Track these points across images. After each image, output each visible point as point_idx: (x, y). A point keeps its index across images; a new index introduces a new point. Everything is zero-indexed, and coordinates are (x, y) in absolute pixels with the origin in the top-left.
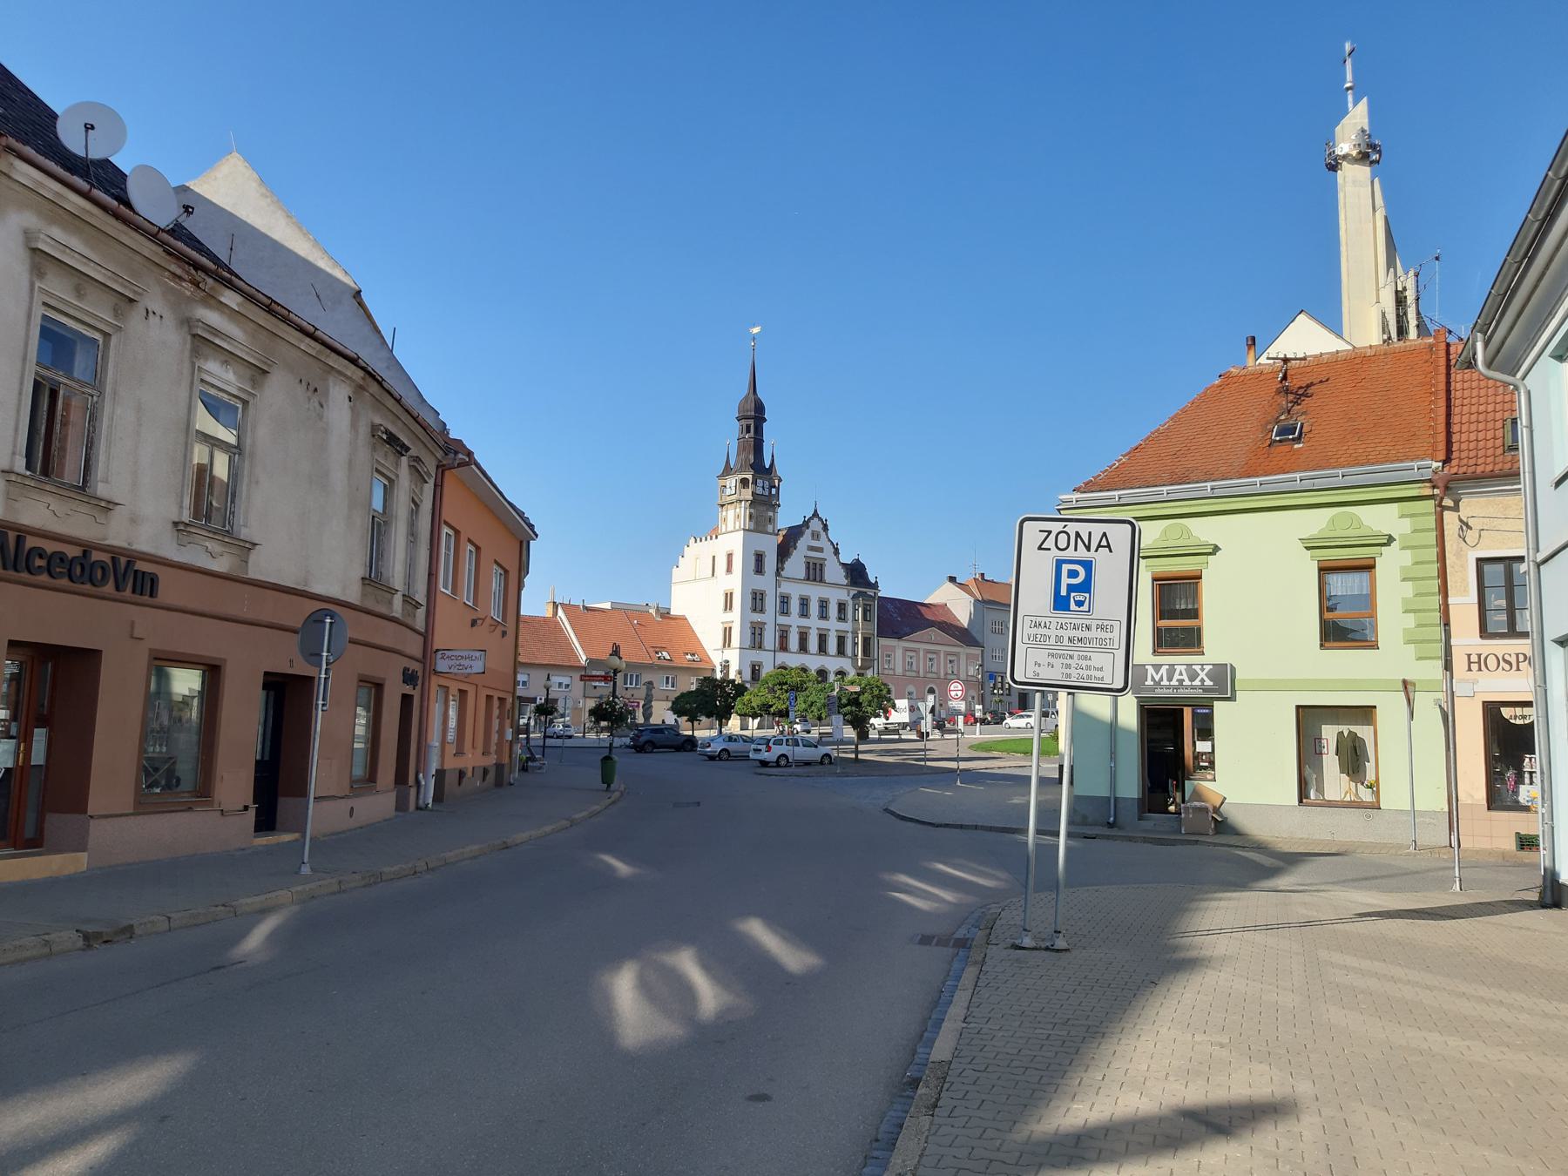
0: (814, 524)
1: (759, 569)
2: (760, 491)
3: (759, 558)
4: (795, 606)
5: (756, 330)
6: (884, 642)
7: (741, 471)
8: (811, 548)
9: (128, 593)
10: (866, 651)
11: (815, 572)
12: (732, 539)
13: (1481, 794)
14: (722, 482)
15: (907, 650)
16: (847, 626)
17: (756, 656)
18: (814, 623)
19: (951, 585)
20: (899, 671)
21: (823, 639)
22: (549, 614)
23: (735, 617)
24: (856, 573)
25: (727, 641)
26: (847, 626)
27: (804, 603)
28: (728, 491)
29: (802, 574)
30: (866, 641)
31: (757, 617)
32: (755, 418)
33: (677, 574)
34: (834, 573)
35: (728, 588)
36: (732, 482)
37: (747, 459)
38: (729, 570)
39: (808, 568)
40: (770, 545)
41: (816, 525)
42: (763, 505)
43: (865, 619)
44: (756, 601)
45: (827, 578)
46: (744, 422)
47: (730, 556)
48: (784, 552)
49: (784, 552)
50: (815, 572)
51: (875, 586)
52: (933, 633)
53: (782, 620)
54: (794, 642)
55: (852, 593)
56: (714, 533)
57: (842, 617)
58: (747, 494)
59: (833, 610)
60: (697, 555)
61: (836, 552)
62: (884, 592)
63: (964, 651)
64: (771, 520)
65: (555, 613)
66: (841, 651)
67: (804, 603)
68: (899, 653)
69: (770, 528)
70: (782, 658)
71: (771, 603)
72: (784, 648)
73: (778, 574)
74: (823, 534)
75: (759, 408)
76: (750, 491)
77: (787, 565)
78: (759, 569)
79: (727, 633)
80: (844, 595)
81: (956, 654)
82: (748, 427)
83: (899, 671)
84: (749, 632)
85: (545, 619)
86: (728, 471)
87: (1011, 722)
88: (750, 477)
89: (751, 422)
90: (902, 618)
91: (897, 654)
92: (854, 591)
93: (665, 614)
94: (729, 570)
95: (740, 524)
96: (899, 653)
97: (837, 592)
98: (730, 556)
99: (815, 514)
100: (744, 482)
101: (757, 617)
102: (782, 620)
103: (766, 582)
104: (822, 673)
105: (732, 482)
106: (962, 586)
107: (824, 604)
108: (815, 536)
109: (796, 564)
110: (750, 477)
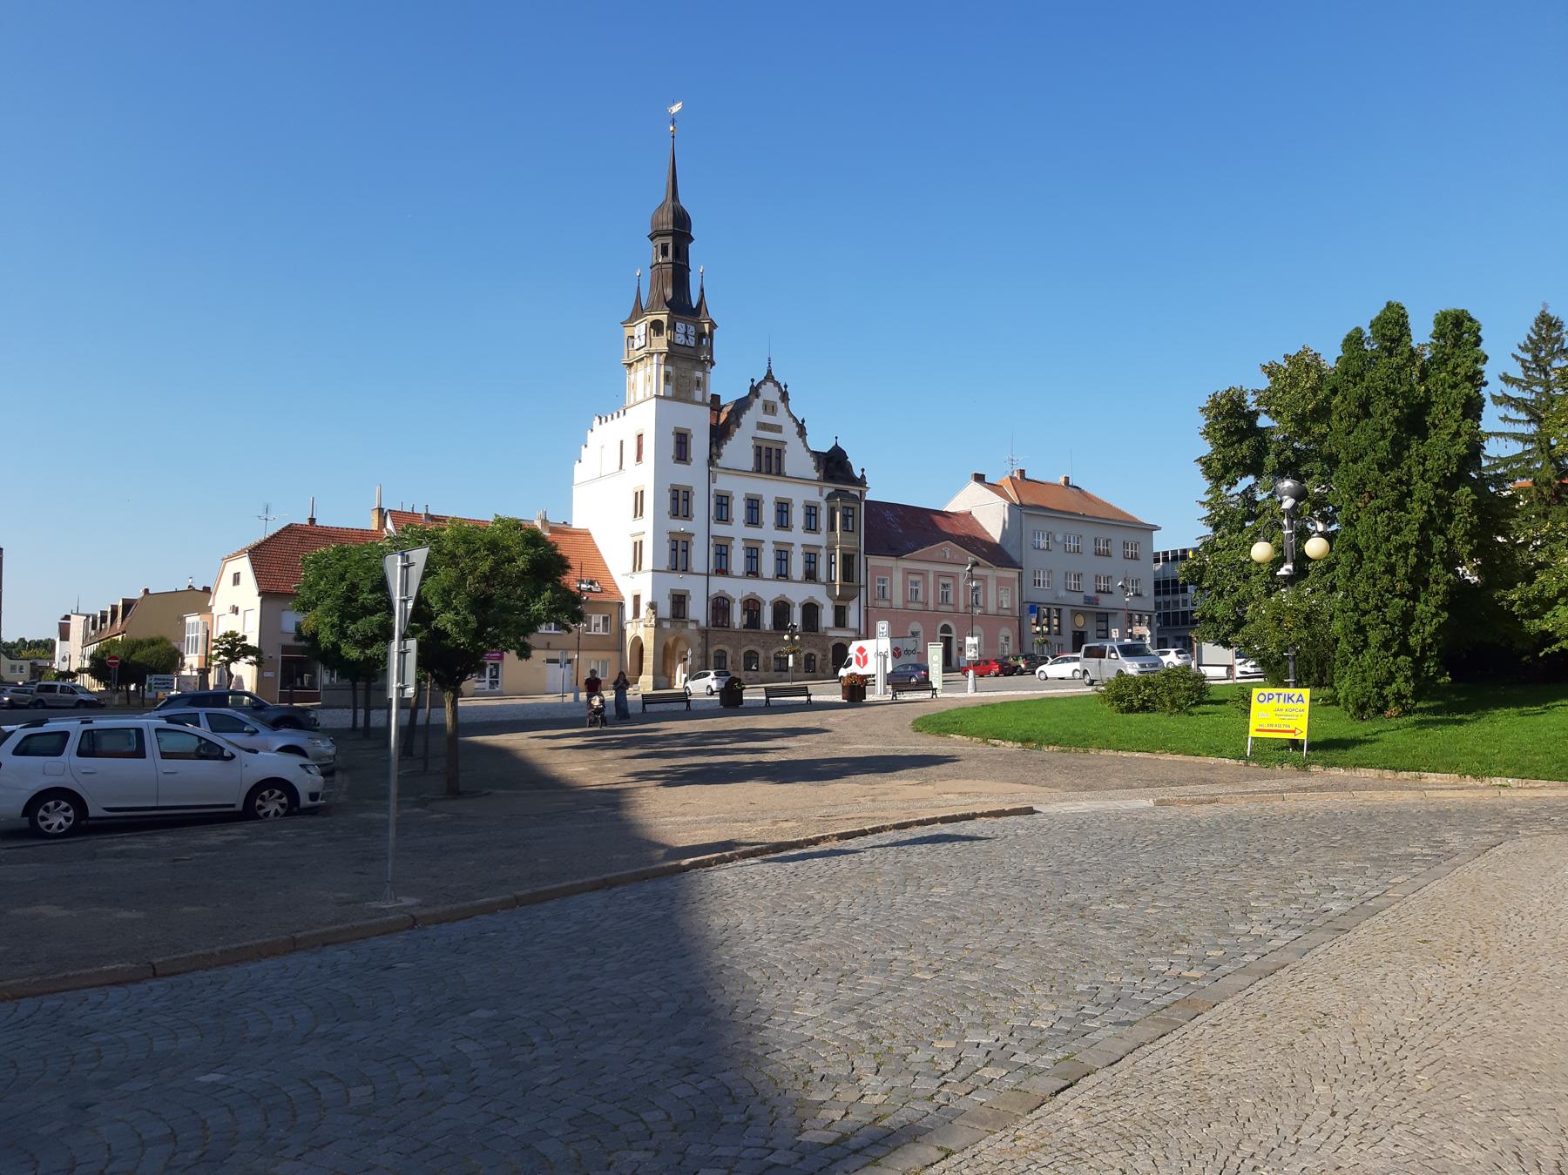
0: (768, 390)
2: (680, 339)
4: (738, 510)
5: (676, 108)
6: (875, 561)
7: (652, 308)
8: (763, 426)
10: (847, 574)
11: (769, 460)
12: (641, 412)
13: (773, 519)
14: (628, 332)
15: (908, 572)
16: (820, 539)
17: (679, 582)
19: (975, 487)
20: (898, 601)
21: (782, 557)
22: (374, 526)
23: (647, 524)
24: (834, 465)
25: (637, 565)
26: (820, 539)
27: (753, 505)
29: (749, 463)
30: (848, 560)
31: (680, 526)
32: (674, 234)
33: (580, 472)
34: (798, 462)
36: (640, 329)
39: (758, 455)
40: (698, 421)
41: (770, 393)
42: (687, 360)
44: (679, 502)
45: (788, 468)
46: (659, 241)
48: (720, 434)
49: (720, 434)
50: (769, 460)
51: (861, 482)
52: (947, 549)
53: (720, 530)
54: (738, 561)
55: (827, 491)
57: (811, 527)
58: (661, 344)
59: (798, 516)
61: (802, 431)
63: (992, 573)
64: (699, 384)
65: (383, 524)
66: (810, 576)
67: (753, 505)
68: (898, 577)
69: (698, 395)
70: (719, 585)
71: (701, 505)
73: (711, 462)
79: (638, 547)
80: (815, 494)
83: (898, 601)
84: (667, 548)
85: (364, 534)
86: (638, 312)
87: (1051, 670)
88: (664, 318)
89: (669, 240)
90: (907, 530)
92: (829, 488)
94: (639, 458)
96: (898, 577)
97: (802, 488)
98: (640, 437)
99: (769, 377)
100: (656, 326)
101: (680, 526)
102: (720, 530)
103: (693, 475)
104: (782, 609)
105: (640, 329)
106: (995, 488)
107: (783, 508)
108: (769, 408)
109: (739, 450)
110: (664, 318)
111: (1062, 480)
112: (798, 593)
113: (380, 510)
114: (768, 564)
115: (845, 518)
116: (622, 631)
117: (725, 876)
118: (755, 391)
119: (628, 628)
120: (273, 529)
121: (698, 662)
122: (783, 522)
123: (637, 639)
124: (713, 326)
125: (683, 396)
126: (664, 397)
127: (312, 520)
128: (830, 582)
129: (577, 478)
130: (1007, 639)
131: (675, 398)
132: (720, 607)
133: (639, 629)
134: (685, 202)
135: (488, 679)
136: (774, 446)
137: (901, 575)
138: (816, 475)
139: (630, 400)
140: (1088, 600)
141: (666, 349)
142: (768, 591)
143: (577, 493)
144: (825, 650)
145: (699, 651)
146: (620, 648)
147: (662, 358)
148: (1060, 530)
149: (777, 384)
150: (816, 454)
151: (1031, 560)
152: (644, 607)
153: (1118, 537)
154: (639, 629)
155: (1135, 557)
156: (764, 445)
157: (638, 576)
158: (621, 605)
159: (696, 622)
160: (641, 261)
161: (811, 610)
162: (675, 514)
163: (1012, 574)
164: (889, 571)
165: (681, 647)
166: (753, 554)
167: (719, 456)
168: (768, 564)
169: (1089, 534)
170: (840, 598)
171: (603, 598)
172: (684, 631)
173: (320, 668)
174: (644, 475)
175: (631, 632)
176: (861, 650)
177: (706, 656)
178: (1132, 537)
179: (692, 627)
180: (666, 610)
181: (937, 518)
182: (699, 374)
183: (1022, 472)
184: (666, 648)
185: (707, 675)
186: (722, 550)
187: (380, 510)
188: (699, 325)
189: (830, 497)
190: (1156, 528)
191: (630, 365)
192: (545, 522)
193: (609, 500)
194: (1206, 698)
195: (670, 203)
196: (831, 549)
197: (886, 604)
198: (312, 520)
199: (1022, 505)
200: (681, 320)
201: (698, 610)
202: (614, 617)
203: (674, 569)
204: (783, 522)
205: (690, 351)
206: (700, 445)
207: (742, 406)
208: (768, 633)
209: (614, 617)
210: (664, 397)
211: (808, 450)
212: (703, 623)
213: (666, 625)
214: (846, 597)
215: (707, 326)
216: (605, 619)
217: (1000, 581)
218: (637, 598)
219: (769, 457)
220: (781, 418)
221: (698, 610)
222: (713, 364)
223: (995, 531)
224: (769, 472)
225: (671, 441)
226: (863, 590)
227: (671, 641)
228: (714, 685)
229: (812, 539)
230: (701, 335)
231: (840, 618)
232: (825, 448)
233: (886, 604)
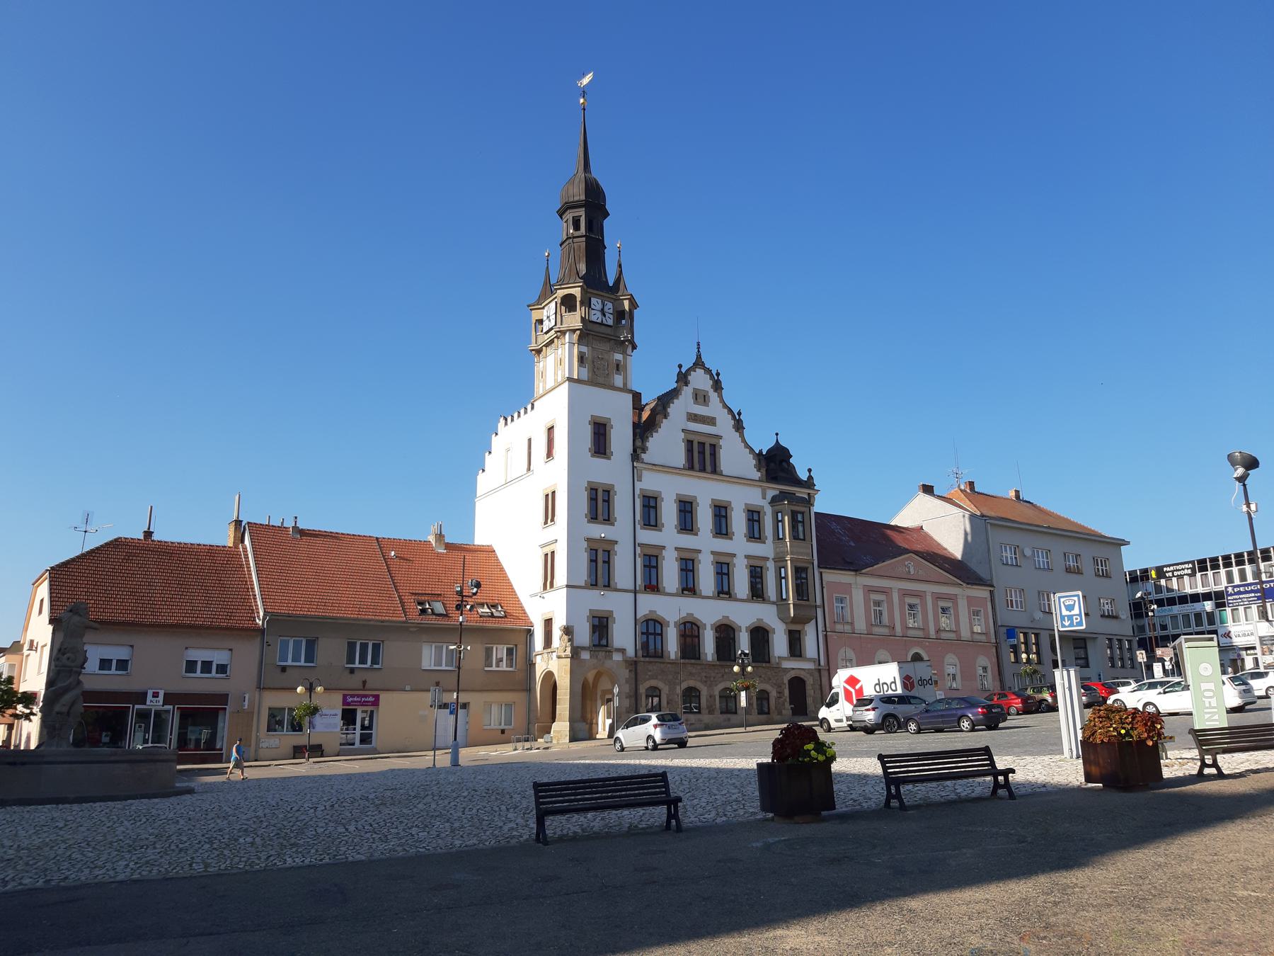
2: (596, 317)
4: (669, 513)
5: (586, 80)
6: (832, 576)
7: (562, 283)
8: (693, 418)
10: (802, 590)
11: (702, 456)
12: (553, 404)
14: (536, 315)
15: (870, 590)
16: (765, 549)
18: (705, 541)
19: (927, 497)
20: (861, 625)
21: (723, 570)
24: (776, 464)
25: (548, 580)
26: (765, 549)
27: (686, 509)
28: (546, 327)
29: (680, 459)
30: (799, 571)
31: (600, 531)
33: (484, 482)
36: (549, 311)
39: (690, 450)
41: (700, 380)
43: (795, 537)
44: (598, 503)
46: (569, 215)
48: (643, 431)
49: (643, 431)
50: (702, 456)
54: (670, 575)
55: (771, 493)
57: (755, 534)
58: (574, 320)
59: (738, 522)
61: (739, 426)
62: (822, 504)
63: (964, 593)
66: (757, 593)
67: (686, 509)
68: (858, 596)
69: (618, 380)
70: (649, 604)
71: (623, 506)
72: (653, 586)
73: (636, 454)
74: (713, 396)
76: (579, 312)
77: (654, 442)
79: (549, 560)
80: (758, 496)
81: (952, 598)
83: (861, 625)
84: (584, 558)
86: (548, 290)
88: (577, 292)
89: (581, 212)
90: (861, 545)
91: (853, 593)
94: (550, 454)
96: (858, 596)
98: (551, 430)
99: (699, 363)
100: (568, 303)
101: (600, 531)
102: (647, 536)
105: (549, 311)
107: (721, 513)
109: (668, 443)
110: (577, 292)
111: (1012, 494)
112: (744, 615)
113: (238, 523)
114: (706, 578)
115: (794, 524)
116: (531, 666)
117: (583, 584)
118: (683, 378)
119: (538, 660)
120: (94, 542)
121: (627, 703)
122: (722, 526)
123: (549, 675)
124: (634, 305)
125: (601, 380)
126: (578, 381)
127: (148, 534)
128: (781, 602)
129: (480, 490)
130: (985, 669)
131: (592, 382)
132: (651, 629)
133: (552, 663)
134: (596, 173)
135: (358, 731)
136: (708, 441)
137: (861, 592)
138: (757, 475)
139: (539, 388)
141: (579, 325)
142: (709, 612)
143: (478, 505)
144: (779, 686)
145: (627, 688)
146: (528, 688)
147: (575, 336)
148: (1028, 544)
149: (708, 371)
151: (1002, 577)
152: (557, 633)
153: (1088, 553)
154: (552, 663)
155: (1106, 575)
156: (696, 439)
157: (550, 595)
158: (529, 633)
159: (623, 651)
160: (551, 238)
161: (760, 635)
162: (593, 517)
163: (981, 593)
164: (848, 588)
165: (604, 684)
166: (688, 566)
167: (644, 450)
168: (706, 578)
169: (1058, 547)
170: (795, 620)
171: (508, 625)
172: (608, 664)
174: (555, 474)
175: (541, 666)
176: (852, 681)
177: (635, 696)
178: (1101, 552)
179: (617, 657)
180: (584, 636)
181: (889, 532)
182: (618, 357)
183: (971, 484)
184: (585, 686)
185: (645, 720)
186: (651, 561)
187: (238, 523)
188: (617, 301)
189: (774, 501)
190: (616, 542)
191: (539, 351)
192: (440, 537)
193: (518, 509)
195: (581, 175)
196: (780, 561)
197: (848, 628)
198: (148, 534)
199: (983, 516)
200: (597, 296)
201: (624, 636)
202: (521, 648)
203: (593, 584)
204: (722, 526)
205: (608, 331)
206: (621, 438)
207: (665, 400)
208: (711, 666)
209: (521, 648)
210: (578, 381)
212: (631, 652)
213: (585, 655)
214: (801, 619)
215: (626, 303)
216: (510, 652)
217: (970, 600)
218: (548, 623)
219: (702, 453)
220: (714, 408)
221: (624, 636)
222: (634, 347)
223: (954, 546)
224: (703, 470)
225: (588, 432)
226: (819, 611)
227: (591, 676)
228: (658, 735)
229: (757, 549)
230: (620, 315)
231: (795, 647)
232: (764, 445)
233: (848, 628)
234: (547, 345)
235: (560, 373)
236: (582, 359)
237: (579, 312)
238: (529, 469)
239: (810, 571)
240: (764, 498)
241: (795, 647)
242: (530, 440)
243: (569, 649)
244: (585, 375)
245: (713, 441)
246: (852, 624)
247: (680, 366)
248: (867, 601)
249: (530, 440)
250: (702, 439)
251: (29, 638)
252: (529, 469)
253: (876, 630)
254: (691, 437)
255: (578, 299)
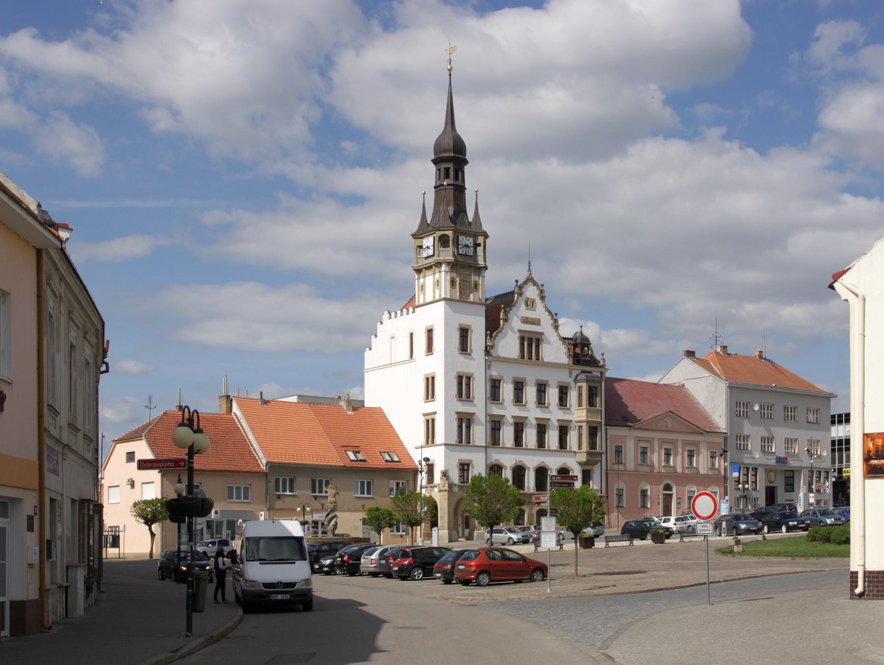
1: (464, 347)
3: (464, 333)
6: (613, 431)
8: (526, 321)
9: (242, 500)
11: (531, 343)
15: (639, 440)
17: (465, 456)
19: (687, 362)
23: (438, 406)
24: (580, 351)
34: (555, 352)
35: (429, 371)
37: (446, 211)
38: (430, 349)
41: (531, 292)
42: (466, 268)
44: (463, 385)
46: (443, 166)
47: (430, 332)
49: (493, 326)
50: (531, 343)
53: (496, 411)
55: (574, 374)
56: (411, 304)
58: (448, 255)
60: (394, 332)
65: (230, 409)
71: (479, 389)
73: (487, 352)
75: (459, 147)
78: (464, 347)
79: (430, 425)
82: (447, 170)
92: (577, 370)
93: (357, 406)
94: (430, 349)
95: (444, 290)
98: (430, 332)
99: (530, 280)
100: (443, 241)
106: (704, 364)
109: (508, 345)
110: (450, 233)
113: (228, 397)
129: (367, 365)
134: (463, 128)
136: (534, 337)
140: (780, 460)
141: (451, 258)
150: (564, 339)
156: (526, 336)
173: (549, 523)
174: (436, 364)
183: (724, 348)
186: (495, 425)
194: (572, 342)
211: (559, 335)
225: (457, 335)
226: (604, 456)
234: (426, 268)
235: (437, 292)
236: (453, 282)
237: (451, 249)
238: (411, 356)
239: (599, 389)
240: (570, 376)
241: (587, 476)
242: (412, 334)
243: (447, 486)
244: (457, 296)
245: (537, 337)
246: (625, 465)
247: (517, 281)
248: (636, 445)
249: (412, 334)
250: (531, 336)
251: (337, 513)
252: (411, 356)
253: (641, 468)
254: (523, 335)
255: (451, 239)
